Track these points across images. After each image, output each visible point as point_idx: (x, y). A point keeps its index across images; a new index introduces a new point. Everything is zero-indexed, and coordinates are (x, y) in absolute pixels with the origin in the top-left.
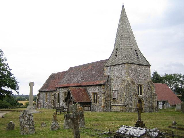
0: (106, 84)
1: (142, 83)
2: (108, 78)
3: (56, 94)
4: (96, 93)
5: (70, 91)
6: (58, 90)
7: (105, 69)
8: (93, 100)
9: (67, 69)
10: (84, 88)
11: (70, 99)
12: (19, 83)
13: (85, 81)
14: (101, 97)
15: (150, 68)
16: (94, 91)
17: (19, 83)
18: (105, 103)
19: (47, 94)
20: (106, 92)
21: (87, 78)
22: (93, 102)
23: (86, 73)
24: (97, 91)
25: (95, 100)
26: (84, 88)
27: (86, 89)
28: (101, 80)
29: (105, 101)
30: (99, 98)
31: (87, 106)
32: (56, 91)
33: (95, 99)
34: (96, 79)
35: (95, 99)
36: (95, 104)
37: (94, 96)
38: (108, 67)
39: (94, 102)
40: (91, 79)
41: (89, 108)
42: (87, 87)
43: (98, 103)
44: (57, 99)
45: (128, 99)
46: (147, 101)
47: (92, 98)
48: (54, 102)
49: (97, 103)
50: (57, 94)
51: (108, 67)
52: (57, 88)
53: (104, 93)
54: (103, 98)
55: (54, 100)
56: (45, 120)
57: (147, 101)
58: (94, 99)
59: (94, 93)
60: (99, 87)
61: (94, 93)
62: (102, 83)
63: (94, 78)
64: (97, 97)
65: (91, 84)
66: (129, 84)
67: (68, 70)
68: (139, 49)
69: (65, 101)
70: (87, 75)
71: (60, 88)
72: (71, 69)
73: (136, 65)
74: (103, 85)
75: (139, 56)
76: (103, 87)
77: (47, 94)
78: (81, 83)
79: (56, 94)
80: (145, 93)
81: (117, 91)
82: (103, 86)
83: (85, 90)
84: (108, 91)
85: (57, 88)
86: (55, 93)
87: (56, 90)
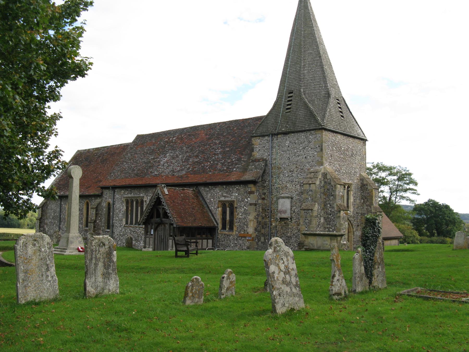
0: (260, 180)
1: (350, 182)
2: (266, 165)
3: (99, 204)
4: (231, 204)
5: (161, 197)
6: (108, 195)
7: (257, 142)
8: (220, 221)
9: (129, 139)
10: (193, 190)
11: (158, 216)
12: (86, 31)
13: (195, 173)
14: (246, 213)
15: (365, 145)
16: (223, 199)
17: (86, 31)
18: (256, 229)
19: (88, 204)
20: (260, 201)
21: (199, 163)
22: (220, 226)
23: (192, 150)
24: (233, 198)
25: (227, 222)
26: (193, 190)
27: (199, 192)
28: (245, 170)
29: (256, 224)
30: (239, 215)
31: (204, 236)
32: (100, 196)
33: (228, 218)
34: (227, 168)
35: (228, 218)
36: (226, 232)
37: (224, 213)
38: (264, 136)
39: (224, 228)
40: (211, 166)
41: (210, 241)
42: (202, 189)
43: (235, 229)
44: (104, 219)
45: (322, 220)
46: (358, 226)
47: (219, 217)
48: (94, 227)
49: (231, 229)
50: (104, 204)
51: (266, 138)
52: (107, 188)
53: (255, 205)
54: (251, 217)
55: (95, 221)
56: (76, 268)
57: (358, 226)
58: (224, 219)
59: (224, 205)
60: (242, 188)
61: (224, 205)
62: (248, 177)
63: (223, 164)
64: (232, 213)
65: (214, 181)
66: (325, 182)
67: (134, 141)
68: (344, 97)
69: (144, 224)
70: (197, 156)
71: (114, 188)
72: (140, 138)
73: (339, 136)
74: (254, 182)
75: (344, 115)
76: (252, 187)
77: (88, 204)
78: (182, 177)
79: (99, 204)
80: (356, 206)
81: (292, 198)
82: (251, 185)
83: (198, 195)
84: (263, 199)
85: (107, 188)
86: (98, 200)
87: (102, 193)
